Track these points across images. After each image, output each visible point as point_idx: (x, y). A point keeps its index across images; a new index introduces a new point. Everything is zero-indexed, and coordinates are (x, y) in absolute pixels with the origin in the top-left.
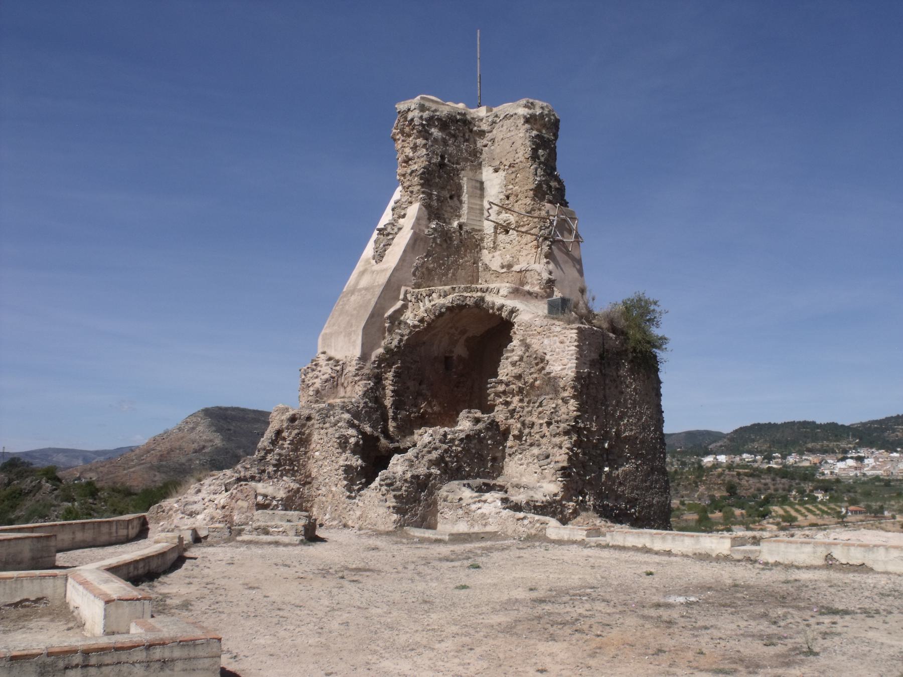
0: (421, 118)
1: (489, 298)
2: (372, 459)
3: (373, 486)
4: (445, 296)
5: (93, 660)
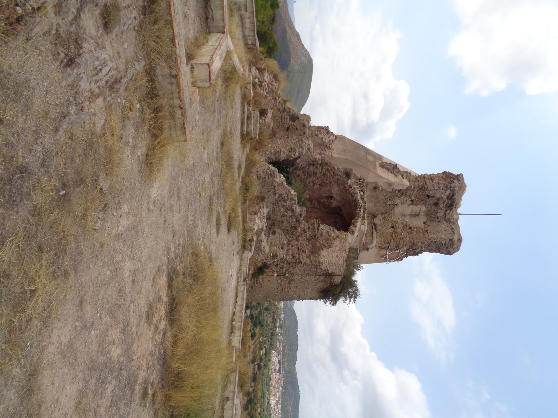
0: (455, 187)
1: (360, 220)
2: (283, 166)
3: (271, 166)
4: (362, 199)
5: (173, 80)
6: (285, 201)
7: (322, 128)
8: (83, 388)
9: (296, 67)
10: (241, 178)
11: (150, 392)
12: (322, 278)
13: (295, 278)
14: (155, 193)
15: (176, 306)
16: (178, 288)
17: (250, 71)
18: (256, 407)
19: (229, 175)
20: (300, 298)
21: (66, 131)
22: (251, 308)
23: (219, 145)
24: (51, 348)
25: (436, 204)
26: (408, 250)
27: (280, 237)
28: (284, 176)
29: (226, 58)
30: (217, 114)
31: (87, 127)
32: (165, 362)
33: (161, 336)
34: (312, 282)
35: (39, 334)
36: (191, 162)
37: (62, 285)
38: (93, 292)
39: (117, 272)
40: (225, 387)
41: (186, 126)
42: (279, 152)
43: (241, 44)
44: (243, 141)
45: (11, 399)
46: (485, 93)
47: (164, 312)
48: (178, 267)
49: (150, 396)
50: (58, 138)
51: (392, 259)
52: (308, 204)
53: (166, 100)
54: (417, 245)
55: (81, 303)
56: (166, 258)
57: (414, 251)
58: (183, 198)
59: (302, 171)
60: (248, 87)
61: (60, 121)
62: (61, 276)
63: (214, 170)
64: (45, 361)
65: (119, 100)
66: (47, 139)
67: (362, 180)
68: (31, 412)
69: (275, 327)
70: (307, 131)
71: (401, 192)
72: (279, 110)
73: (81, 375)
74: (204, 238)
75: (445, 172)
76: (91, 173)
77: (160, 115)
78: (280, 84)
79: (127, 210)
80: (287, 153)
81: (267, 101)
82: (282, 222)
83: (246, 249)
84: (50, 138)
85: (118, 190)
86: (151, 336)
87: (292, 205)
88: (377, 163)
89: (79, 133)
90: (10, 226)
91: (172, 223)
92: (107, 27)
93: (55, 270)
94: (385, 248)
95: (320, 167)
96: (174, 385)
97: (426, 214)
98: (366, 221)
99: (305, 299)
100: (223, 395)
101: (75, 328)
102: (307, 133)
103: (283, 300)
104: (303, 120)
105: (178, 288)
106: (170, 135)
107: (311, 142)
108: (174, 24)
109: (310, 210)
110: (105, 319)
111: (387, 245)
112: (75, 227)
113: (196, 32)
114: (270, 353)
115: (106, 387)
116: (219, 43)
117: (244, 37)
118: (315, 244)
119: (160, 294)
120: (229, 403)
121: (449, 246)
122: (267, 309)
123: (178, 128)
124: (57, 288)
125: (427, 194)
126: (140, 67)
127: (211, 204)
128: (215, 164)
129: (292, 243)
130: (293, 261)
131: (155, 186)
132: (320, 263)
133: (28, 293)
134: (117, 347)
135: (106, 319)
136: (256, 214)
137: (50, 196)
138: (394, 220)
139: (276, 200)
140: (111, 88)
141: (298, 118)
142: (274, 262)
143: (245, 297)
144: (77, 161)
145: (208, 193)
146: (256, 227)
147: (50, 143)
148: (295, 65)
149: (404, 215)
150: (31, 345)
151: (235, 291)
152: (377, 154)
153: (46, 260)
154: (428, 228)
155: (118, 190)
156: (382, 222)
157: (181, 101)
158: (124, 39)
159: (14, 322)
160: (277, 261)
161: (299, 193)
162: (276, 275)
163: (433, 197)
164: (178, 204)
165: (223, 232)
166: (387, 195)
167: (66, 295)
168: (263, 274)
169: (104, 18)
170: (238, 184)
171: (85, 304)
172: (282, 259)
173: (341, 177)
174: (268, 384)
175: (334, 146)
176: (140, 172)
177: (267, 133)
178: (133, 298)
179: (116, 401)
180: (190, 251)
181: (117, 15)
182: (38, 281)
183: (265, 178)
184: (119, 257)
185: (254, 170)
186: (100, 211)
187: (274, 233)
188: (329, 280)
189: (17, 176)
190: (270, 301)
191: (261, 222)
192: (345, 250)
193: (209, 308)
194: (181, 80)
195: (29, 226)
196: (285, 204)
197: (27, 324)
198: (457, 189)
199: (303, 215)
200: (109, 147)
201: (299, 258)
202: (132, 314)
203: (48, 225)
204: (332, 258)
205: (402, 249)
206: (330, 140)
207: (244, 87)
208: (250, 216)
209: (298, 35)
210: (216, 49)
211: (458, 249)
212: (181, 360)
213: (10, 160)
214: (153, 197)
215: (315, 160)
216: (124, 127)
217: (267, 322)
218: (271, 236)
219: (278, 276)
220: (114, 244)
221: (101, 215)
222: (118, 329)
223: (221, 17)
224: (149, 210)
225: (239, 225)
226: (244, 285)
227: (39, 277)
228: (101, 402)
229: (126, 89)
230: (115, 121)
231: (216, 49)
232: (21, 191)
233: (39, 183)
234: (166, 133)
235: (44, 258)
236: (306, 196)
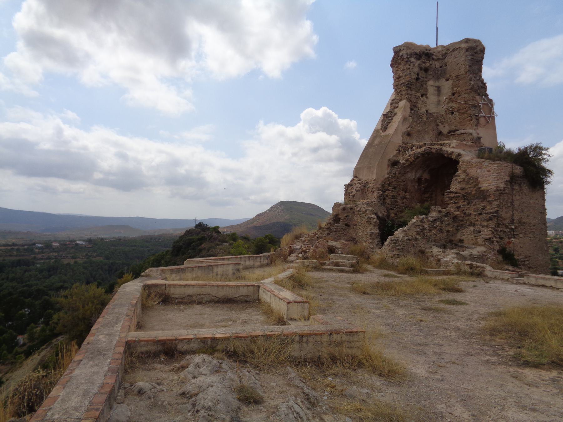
1: (445, 148)
2: (386, 229)
3: (386, 243)
4: (421, 147)
5: (304, 339)
6: (424, 229)
7: (346, 191)
9: (287, 217)
10: (399, 275)
12: (516, 187)
13: (516, 217)
14: (421, 371)
16: (538, 356)
17: (292, 261)
19: (397, 288)
23: (365, 296)
25: (426, 70)
26: (479, 94)
27: (466, 234)
28: (397, 230)
29: (281, 286)
30: (334, 297)
34: (522, 198)
36: (384, 327)
41: (349, 330)
43: (268, 270)
46: (315, 38)
48: (510, 353)
52: (426, 204)
53: (323, 349)
54: (473, 86)
56: (499, 366)
57: (481, 88)
59: (391, 211)
60: (307, 264)
63: (392, 304)
65: (325, 398)
67: (401, 149)
70: (350, 206)
71: (413, 107)
72: (328, 234)
75: (392, 65)
77: (338, 357)
78: (303, 233)
79: (443, 405)
80: (372, 226)
81: (320, 246)
82: (448, 231)
83: (481, 273)
87: (428, 221)
88: (382, 134)
91: (455, 355)
92: (258, 401)
94: (478, 120)
95: (387, 192)
97: (439, 81)
98: (446, 142)
102: (351, 206)
105: (538, 356)
107: (360, 202)
108: (254, 334)
109: (434, 202)
113: (258, 313)
116: (268, 291)
117: (261, 266)
118: (474, 196)
119: (547, 378)
121: (474, 52)
122: (556, 250)
123: (351, 339)
125: (414, 81)
126: (293, 373)
127: (431, 309)
129: (473, 221)
130: (495, 220)
131: (413, 370)
132: (497, 190)
136: (439, 260)
138: (444, 113)
139: (424, 238)
140: (313, 405)
141: (337, 215)
142: (497, 242)
143: (543, 276)
145: (418, 312)
146: (455, 261)
148: (285, 218)
149: (439, 102)
151: (535, 288)
152: (372, 135)
154: (453, 75)
155: (420, 413)
156: (446, 125)
157: (325, 334)
158: (267, 385)
160: (496, 238)
162: (513, 239)
163: (418, 74)
164: (432, 346)
166: (416, 122)
168: (513, 255)
169: (250, 402)
170: (407, 278)
172: (493, 233)
173: (397, 171)
175: (364, 178)
176: (399, 385)
178: (556, 414)
180: (488, 337)
181: (248, 390)
183: (398, 249)
185: (390, 261)
187: (461, 241)
191: (448, 255)
194: (305, 332)
196: (427, 229)
198: (409, 51)
199: (440, 209)
200: (373, 416)
201: (491, 213)
204: (491, 177)
205: (479, 101)
207: (308, 268)
208: (442, 267)
209: (259, 216)
210: (273, 294)
211: (478, 42)
218: (465, 245)
219: (514, 238)
223: (246, 288)
224: (442, 380)
225: (453, 279)
229: (314, 389)
230: (346, 405)
231: (273, 294)
234: (355, 352)
236: (418, 206)
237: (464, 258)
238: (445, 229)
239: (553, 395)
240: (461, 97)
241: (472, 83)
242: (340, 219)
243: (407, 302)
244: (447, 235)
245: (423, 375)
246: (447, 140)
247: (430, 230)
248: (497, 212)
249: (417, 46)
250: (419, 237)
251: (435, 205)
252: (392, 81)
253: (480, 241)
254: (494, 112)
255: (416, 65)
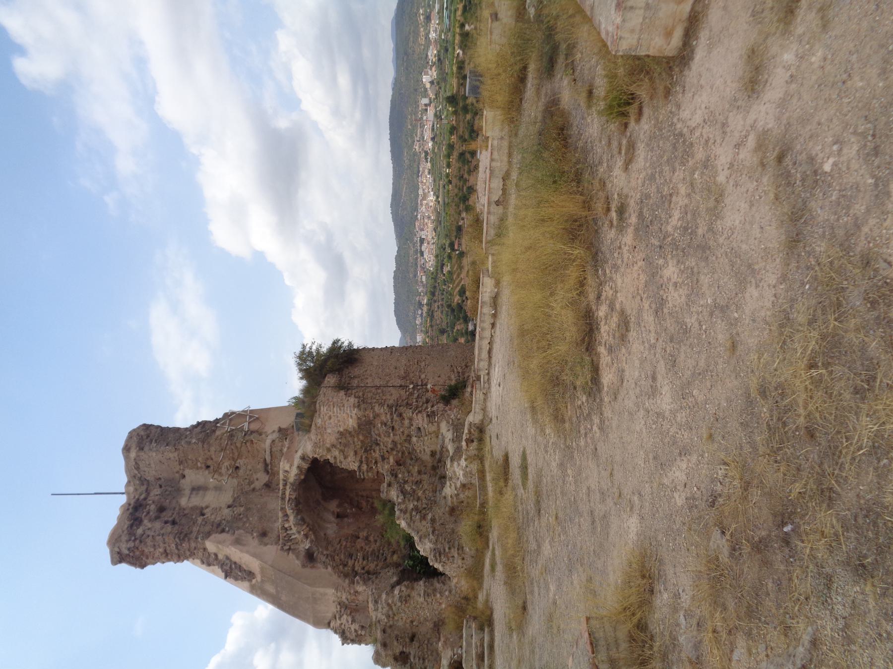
0: (127, 541)
1: (292, 477)
2: (419, 570)
3: (441, 569)
4: (286, 515)
6: (416, 509)
7: (353, 641)
8: (715, 221)
10: (491, 547)
11: (614, 214)
13: (398, 382)
14: (633, 524)
15: (584, 339)
16: (583, 367)
18: (456, 191)
19: (511, 552)
20: (390, 351)
21: (798, 640)
22: (467, 332)
24: (772, 279)
25: (161, 509)
26: (214, 431)
27: (424, 447)
28: (419, 552)
31: (761, 647)
32: (595, 256)
33: (604, 294)
34: (371, 375)
35: (793, 301)
36: (575, 577)
37: (767, 375)
38: (716, 364)
39: (683, 393)
40: (502, 220)
41: (589, 648)
42: (427, 594)
44: (488, 613)
45: (821, 208)
47: (602, 330)
48: (584, 399)
49: (613, 208)
50: (810, 629)
51: (240, 415)
52: (377, 504)
54: (198, 440)
55: (734, 347)
56: (605, 415)
57: (205, 429)
58: (585, 515)
61: (811, 660)
62: (772, 389)
64: (778, 260)
66: (829, 628)
68: (789, 190)
69: (429, 304)
70: (379, 634)
71: (220, 529)
73: (721, 240)
74: (546, 447)
75: (143, 566)
76: (744, 563)
79: (676, 495)
80: (414, 594)
82: (419, 472)
83: (478, 428)
84: (824, 627)
85: (695, 531)
86: (619, 295)
87: (404, 502)
89: (774, 636)
90: (867, 473)
91: (599, 472)
93: (782, 399)
94: (252, 432)
96: (578, 223)
97: (177, 496)
98: (281, 476)
99: (382, 349)
100: (506, 208)
101: (738, 308)
102: (379, 632)
103: (417, 347)
104: (386, 656)
106: (615, 630)
110: (693, 321)
111: (247, 438)
112: (758, 469)
114: (437, 267)
115: (680, 222)
120: (495, 198)
121: (147, 439)
122: (442, 332)
124: (776, 370)
125: (177, 527)
127: (538, 502)
128: (535, 572)
129: (403, 438)
130: (402, 409)
131: (632, 536)
133: (820, 364)
134: (669, 279)
135: (691, 321)
136: (464, 486)
137: (809, 524)
138: (235, 480)
139: (431, 508)
141: (396, 659)
142: (432, 406)
144: (770, 585)
145: (544, 521)
146: (463, 463)
147: (822, 619)
149: (218, 489)
150: (803, 284)
151: (493, 361)
153: (799, 416)
154: (177, 468)
155: (695, 531)
156: (255, 477)
159: (836, 320)
160: (427, 408)
161: (393, 522)
162: (429, 386)
163: (166, 522)
164: (592, 504)
165: (516, 454)
166: (244, 523)
167: (759, 358)
168: (450, 386)
170: (494, 535)
171: (728, 344)
172: (420, 412)
174: (438, 222)
176: (661, 562)
177: (449, 628)
178: (652, 352)
179: (664, 202)
180: (567, 425)
182: (807, 383)
183: (449, 548)
184: (681, 417)
185: (469, 561)
186: (720, 495)
187: (433, 454)
188: (343, 380)
189: (869, 560)
190: (438, 345)
191: (454, 472)
192: (317, 428)
193: (533, 336)
195: (836, 472)
196: (416, 503)
197: (814, 316)
199: (385, 485)
201: (391, 414)
202: (652, 328)
203: (804, 474)
204: (340, 415)
206: (340, 618)
208: (473, 481)
211: (131, 435)
212: (570, 259)
213: (888, 589)
214: (635, 516)
215: (365, 582)
216: (697, 646)
217: (442, 312)
218: (438, 448)
220: (691, 439)
221: (719, 487)
222: (671, 305)
225: (490, 466)
226: (479, 370)
227: (806, 388)
228: (686, 201)
232: (858, 533)
233: (830, 545)
235: (802, 419)
236: (380, 519)
237: (458, 450)
238: (417, 477)
239: (630, 354)
240: (213, 457)
241: (194, 441)
242: (402, 653)
243: (531, 538)
244: (425, 473)
245: (637, 521)
246: (278, 474)
247: (418, 499)
248: (390, 407)
249: (117, 524)
250: (429, 516)
251: (379, 491)
252: (170, 564)
253: (433, 428)
254: (243, 411)
255: (149, 525)
